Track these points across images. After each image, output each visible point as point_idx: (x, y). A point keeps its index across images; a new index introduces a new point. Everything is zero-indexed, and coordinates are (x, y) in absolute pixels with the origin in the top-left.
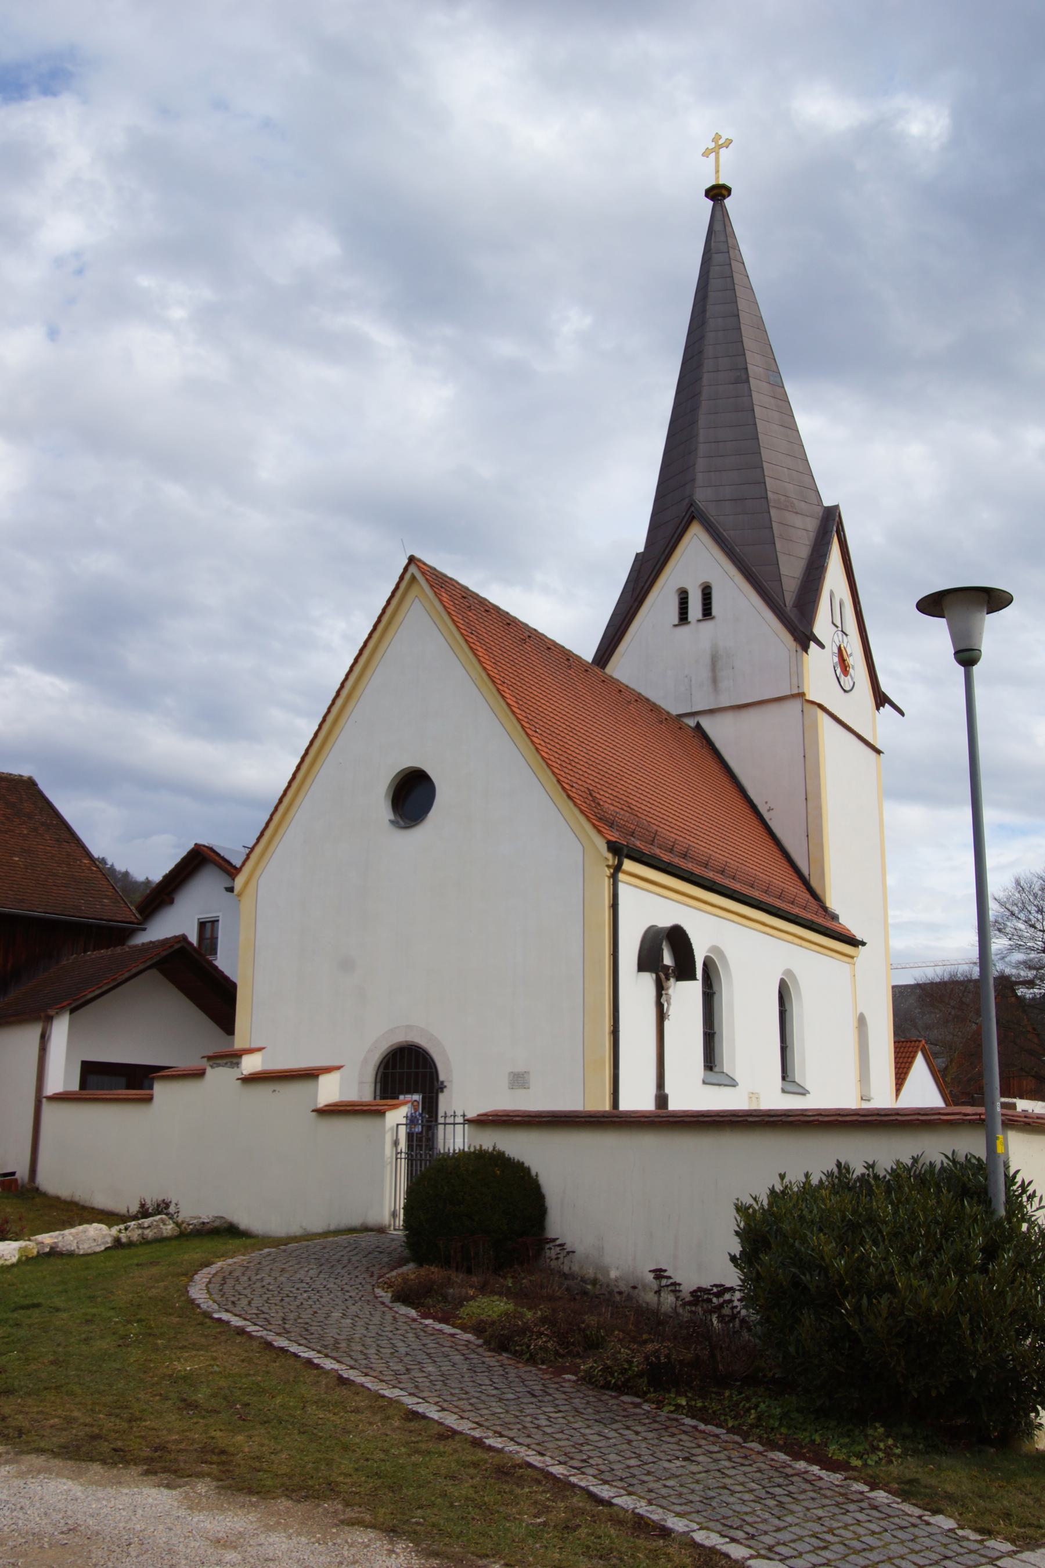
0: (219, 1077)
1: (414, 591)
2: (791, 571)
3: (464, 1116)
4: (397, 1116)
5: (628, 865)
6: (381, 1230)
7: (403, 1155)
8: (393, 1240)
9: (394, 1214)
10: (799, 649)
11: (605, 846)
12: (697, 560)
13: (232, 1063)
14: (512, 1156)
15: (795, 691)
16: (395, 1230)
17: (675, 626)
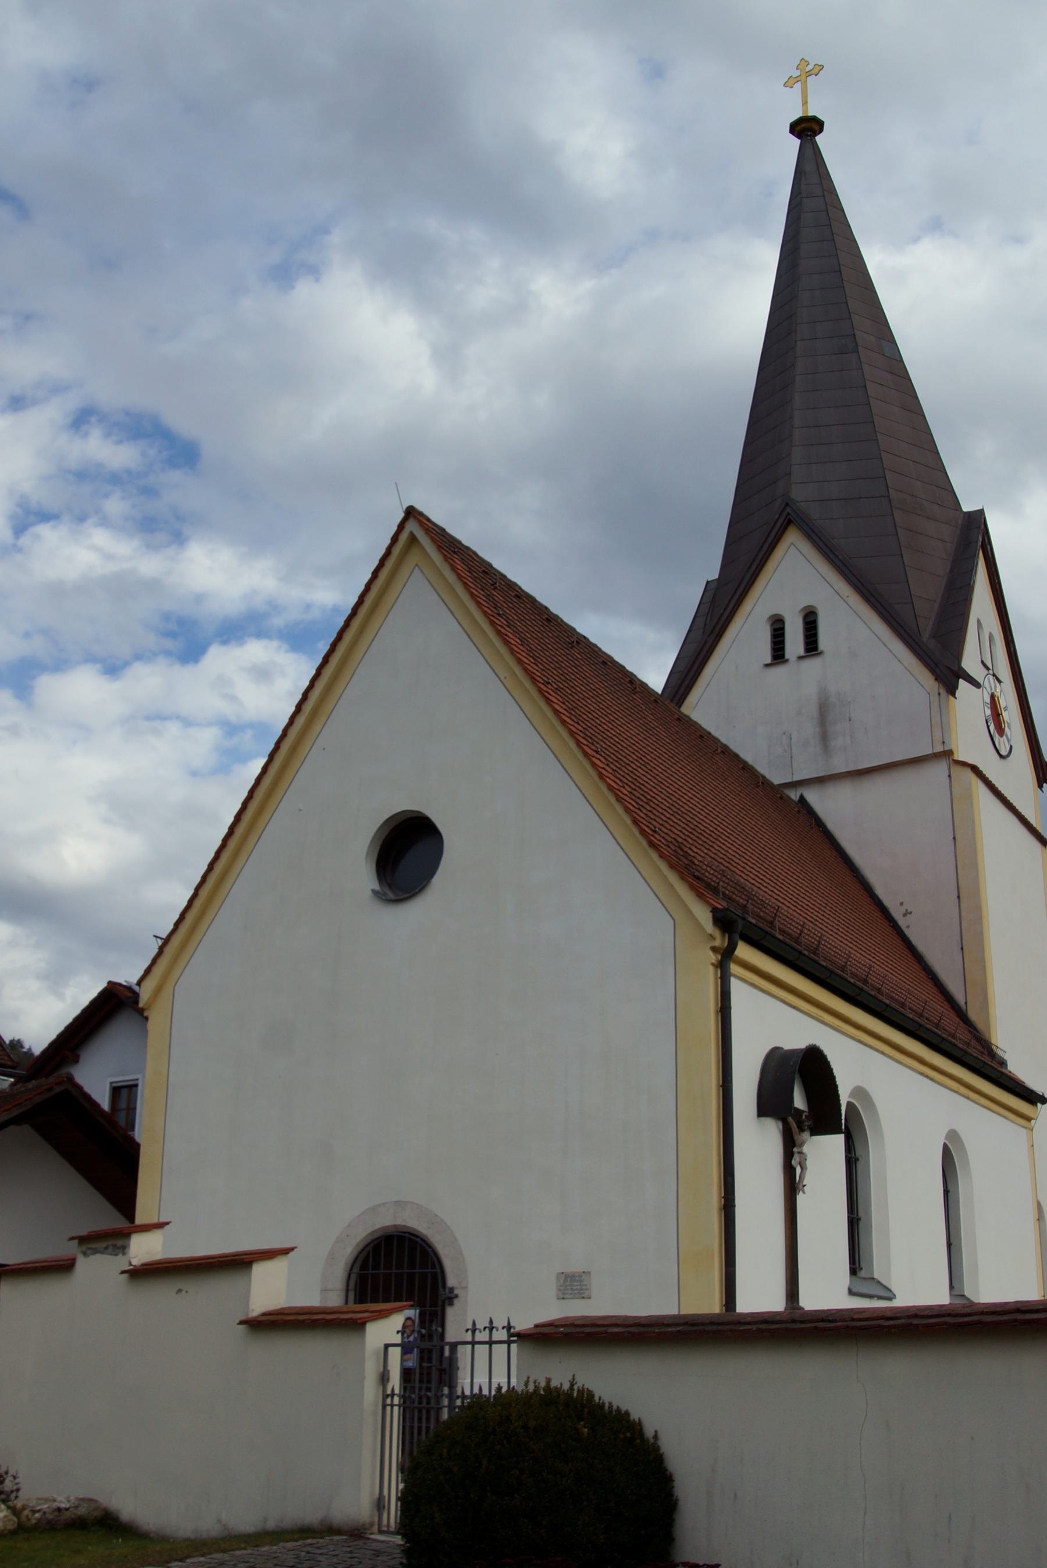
0: (97, 1271)
1: (414, 557)
2: (925, 593)
3: (509, 1327)
4: (386, 1331)
5: (744, 951)
6: (357, 1533)
7: (396, 1400)
8: (378, 1553)
9: (380, 1504)
10: (943, 691)
11: (710, 915)
12: (796, 577)
13: (115, 1246)
14: (606, 1399)
15: (939, 749)
16: (381, 1532)
17: (767, 665)
